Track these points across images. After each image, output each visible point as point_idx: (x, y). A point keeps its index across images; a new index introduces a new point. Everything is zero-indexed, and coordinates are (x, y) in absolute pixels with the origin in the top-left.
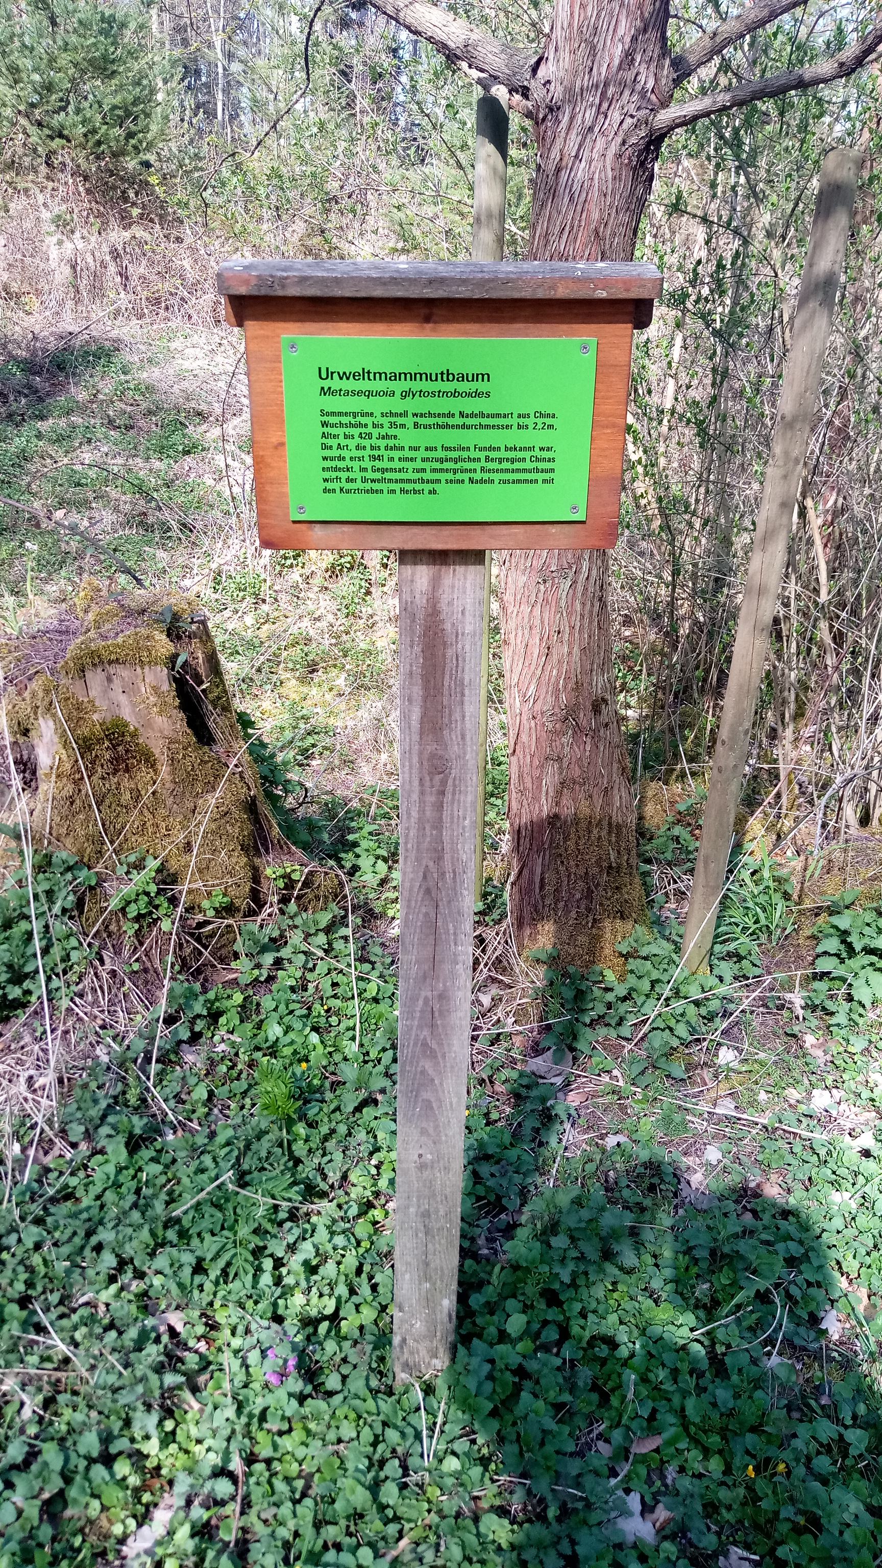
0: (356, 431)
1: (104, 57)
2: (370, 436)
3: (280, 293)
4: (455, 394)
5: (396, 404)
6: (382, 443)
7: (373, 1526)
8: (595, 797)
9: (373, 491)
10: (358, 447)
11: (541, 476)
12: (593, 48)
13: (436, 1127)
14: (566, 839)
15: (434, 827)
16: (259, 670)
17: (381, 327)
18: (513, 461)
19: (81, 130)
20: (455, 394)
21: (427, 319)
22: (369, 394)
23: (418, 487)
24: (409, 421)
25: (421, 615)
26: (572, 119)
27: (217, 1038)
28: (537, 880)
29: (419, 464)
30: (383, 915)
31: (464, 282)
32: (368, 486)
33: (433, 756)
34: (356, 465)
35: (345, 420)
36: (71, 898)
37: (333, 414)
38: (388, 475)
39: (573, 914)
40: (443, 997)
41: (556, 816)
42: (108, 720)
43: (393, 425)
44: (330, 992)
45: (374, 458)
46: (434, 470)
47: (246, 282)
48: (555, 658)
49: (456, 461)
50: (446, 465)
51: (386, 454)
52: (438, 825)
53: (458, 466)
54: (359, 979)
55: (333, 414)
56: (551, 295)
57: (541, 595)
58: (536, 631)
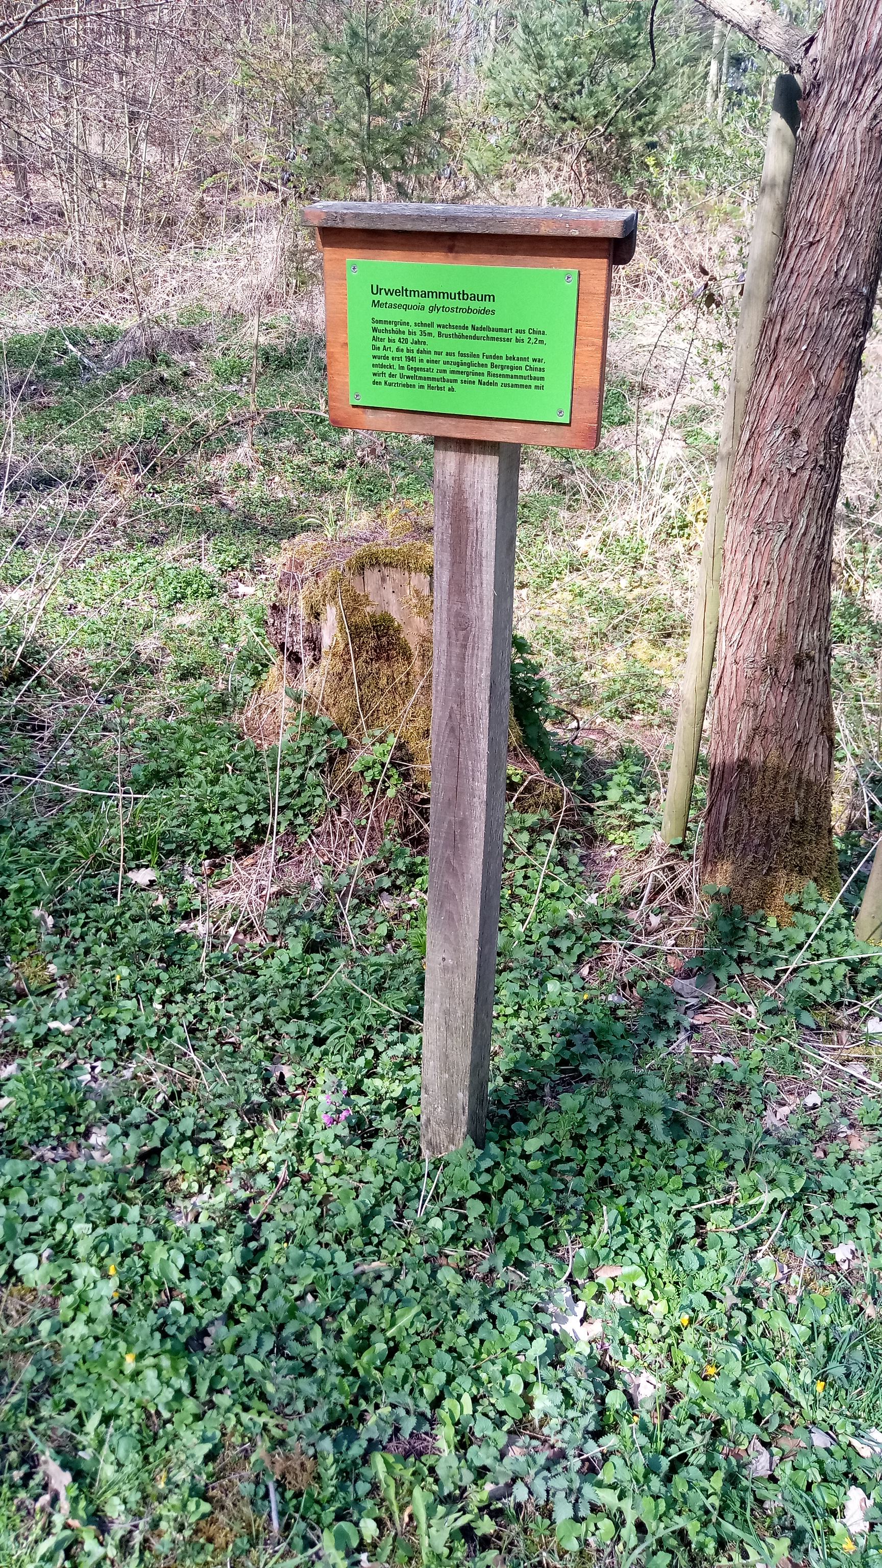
0: (396, 337)
1: (626, 42)
2: (406, 341)
3: (341, 225)
4: (468, 310)
5: (425, 317)
6: (415, 347)
7: (356, 1243)
8: (787, 749)
9: (408, 386)
10: (398, 350)
11: (533, 383)
12: (855, 27)
13: (456, 936)
14: (752, 784)
15: (458, 676)
16: (614, 628)
17: (417, 255)
18: (512, 368)
19: (593, 112)
20: (468, 310)
21: (451, 249)
22: (406, 307)
23: (441, 384)
24: (435, 330)
25: (450, 493)
26: (830, 93)
27: (412, 894)
28: (723, 819)
29: (441, 366)
30: (604, 838)
31: (471, 220)
32: (405, 381)
33: (458, 614)
34: (396, 363)
35: (389, 327)
36: (324, 755)
37: (380, 322)
38: (419, 374)
39: (750, 858)
40: (463, 823)
41: (746, 761)
42: (378, 614)
43: (423, 333)
44: (520, 881)
45: (409, 359)
46: (452, 372)
47: (319, 217)
48: (761, 607)
49: (469, 365)
50: (461, 369)
51: (418, 356)
52: (461, 673)
53: (471, 369)
54: (547, 876)
55: (380, 322)
56: (535, 232)
57: (754, 545)
58: (747, 579)
